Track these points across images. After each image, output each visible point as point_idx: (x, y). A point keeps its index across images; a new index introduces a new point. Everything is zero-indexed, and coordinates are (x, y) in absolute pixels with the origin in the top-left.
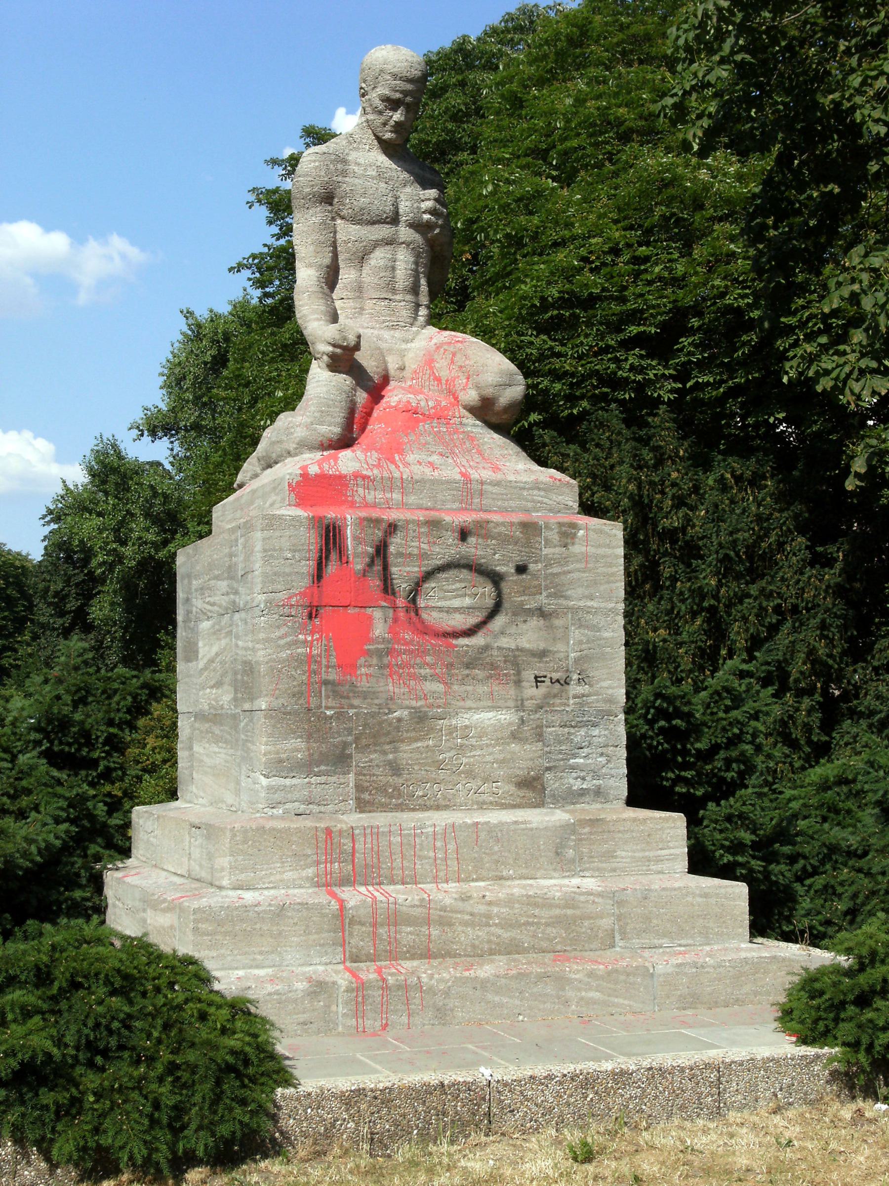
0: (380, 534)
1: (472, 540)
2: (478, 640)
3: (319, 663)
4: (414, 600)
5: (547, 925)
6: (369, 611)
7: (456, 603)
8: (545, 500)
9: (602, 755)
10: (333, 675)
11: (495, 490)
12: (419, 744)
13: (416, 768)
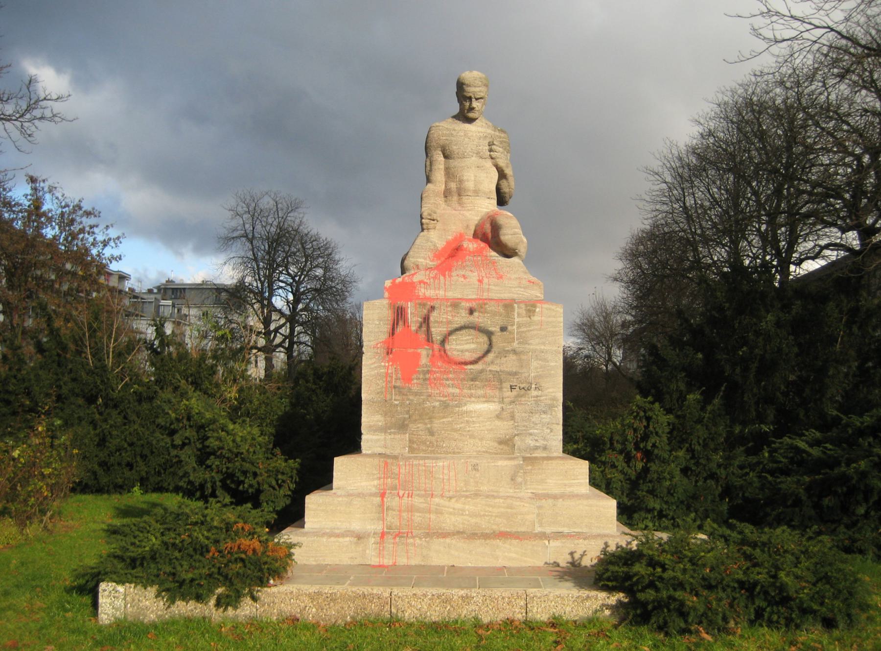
0: (425, 311)
1: (476, 314)
2: (479, 367)
3: (392, 377)
4: (444, 346)
5: (496, 516)
6: (419, 350)
10: (398, 384)
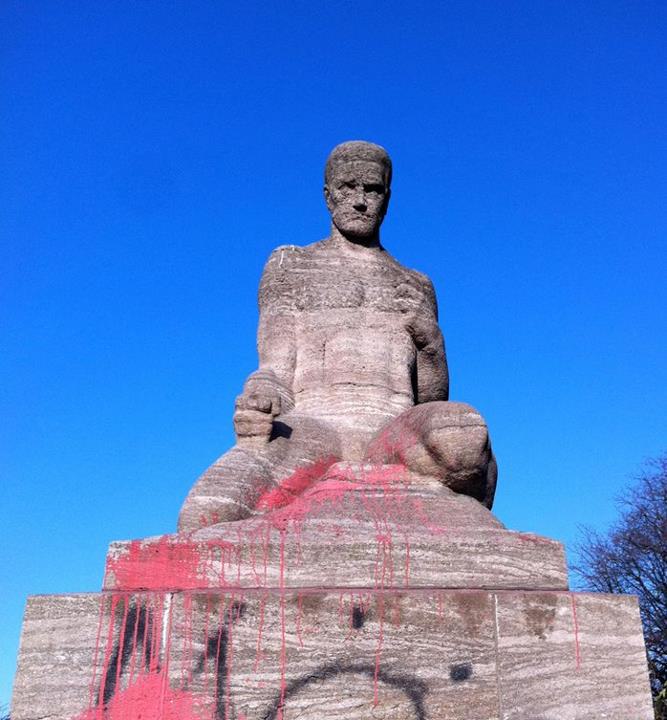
1: (371, 626)
8: (512, 570)
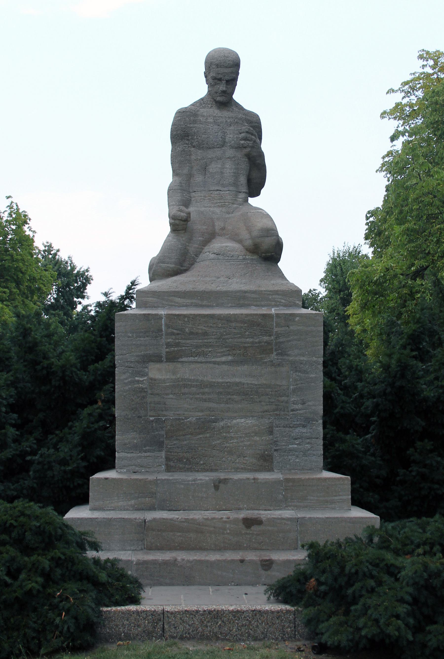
5: (258, 535)
7: (224, 359)
9: (308, 443)
11: (253, 296)
12: (201, 436)
13: (200, 449)
